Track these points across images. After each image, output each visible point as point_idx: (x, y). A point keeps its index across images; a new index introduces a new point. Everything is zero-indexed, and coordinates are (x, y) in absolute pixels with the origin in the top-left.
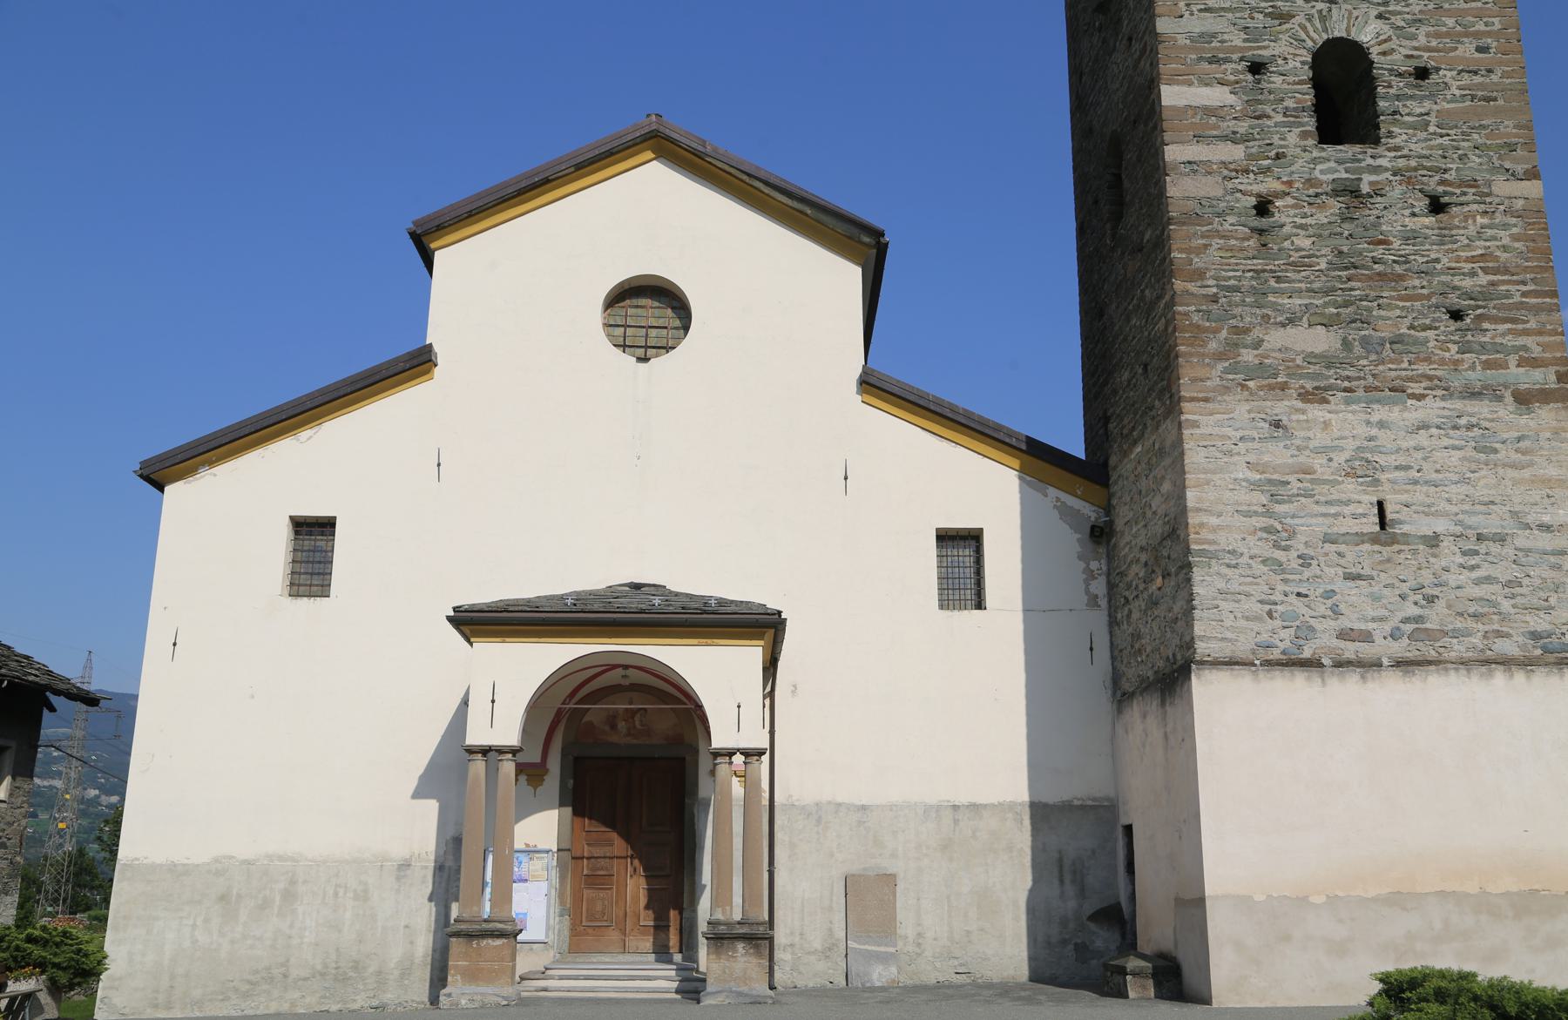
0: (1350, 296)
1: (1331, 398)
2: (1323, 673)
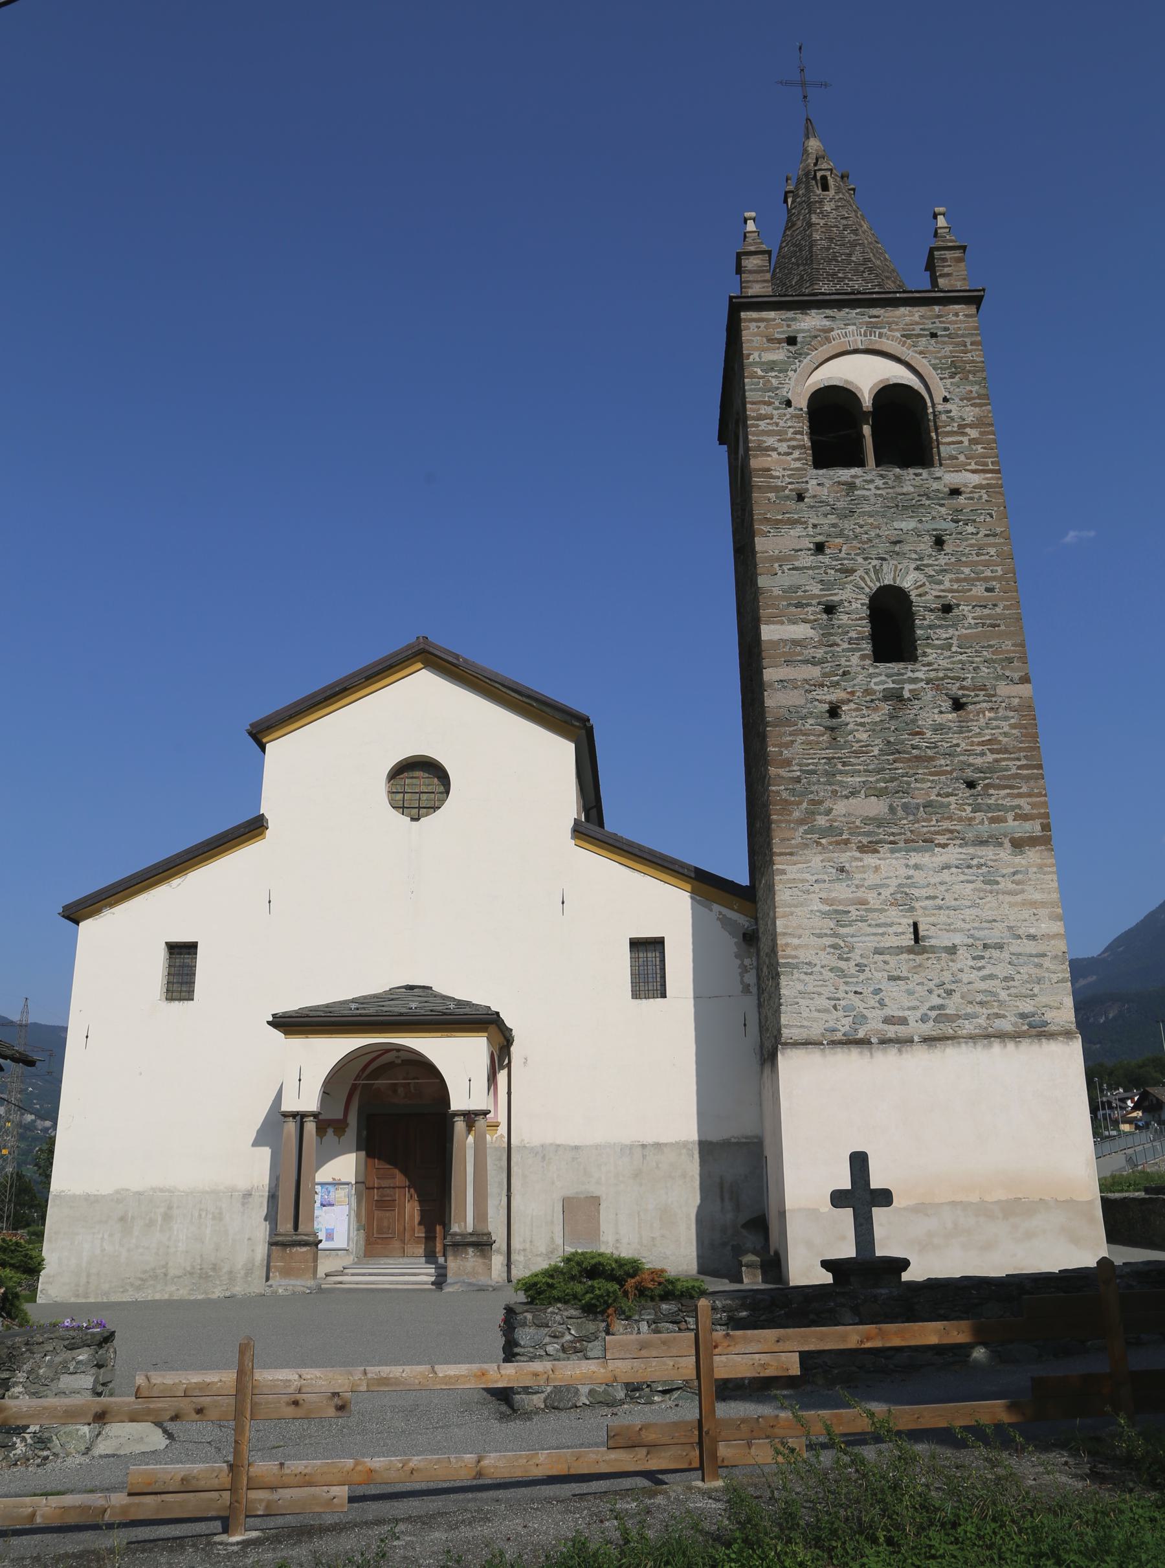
2: (871, 1048)
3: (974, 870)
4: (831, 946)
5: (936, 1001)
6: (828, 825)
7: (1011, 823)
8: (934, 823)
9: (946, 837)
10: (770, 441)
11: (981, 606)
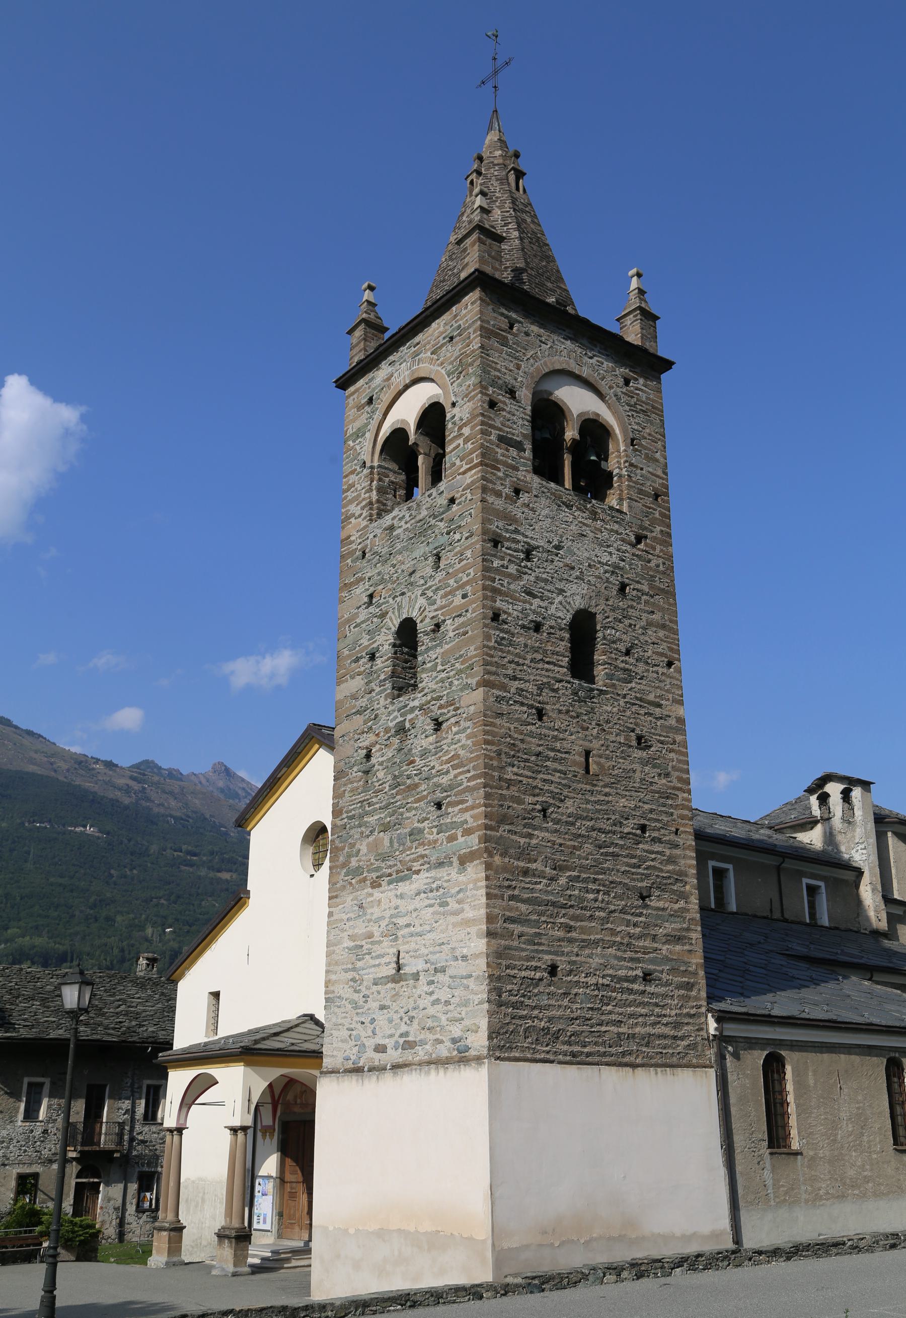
0: (395, 806)
1: (382, 882)
2: (363, 1076)
3: (435, 893)
4: (352, 980)
5: (404, 1028)
6: (357, 865)
7: (461, 840)
8: (413, 850)
9: (419, 863)
10: (520, 422)
11: (458, 616)
